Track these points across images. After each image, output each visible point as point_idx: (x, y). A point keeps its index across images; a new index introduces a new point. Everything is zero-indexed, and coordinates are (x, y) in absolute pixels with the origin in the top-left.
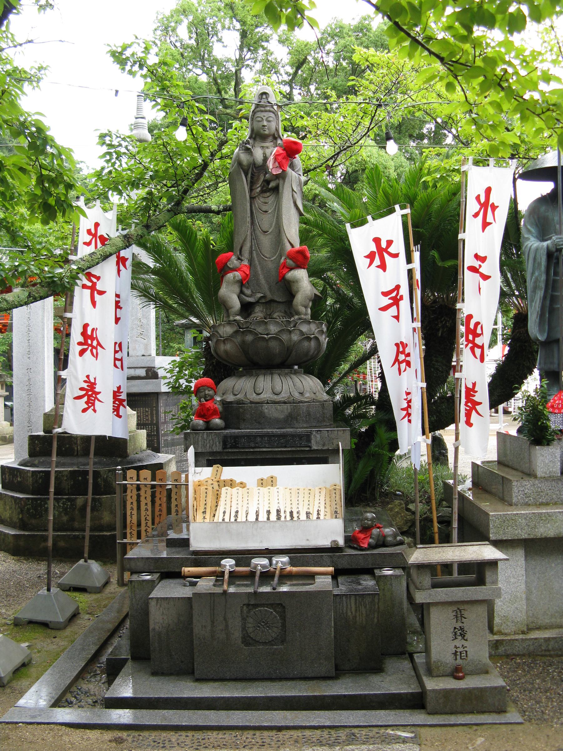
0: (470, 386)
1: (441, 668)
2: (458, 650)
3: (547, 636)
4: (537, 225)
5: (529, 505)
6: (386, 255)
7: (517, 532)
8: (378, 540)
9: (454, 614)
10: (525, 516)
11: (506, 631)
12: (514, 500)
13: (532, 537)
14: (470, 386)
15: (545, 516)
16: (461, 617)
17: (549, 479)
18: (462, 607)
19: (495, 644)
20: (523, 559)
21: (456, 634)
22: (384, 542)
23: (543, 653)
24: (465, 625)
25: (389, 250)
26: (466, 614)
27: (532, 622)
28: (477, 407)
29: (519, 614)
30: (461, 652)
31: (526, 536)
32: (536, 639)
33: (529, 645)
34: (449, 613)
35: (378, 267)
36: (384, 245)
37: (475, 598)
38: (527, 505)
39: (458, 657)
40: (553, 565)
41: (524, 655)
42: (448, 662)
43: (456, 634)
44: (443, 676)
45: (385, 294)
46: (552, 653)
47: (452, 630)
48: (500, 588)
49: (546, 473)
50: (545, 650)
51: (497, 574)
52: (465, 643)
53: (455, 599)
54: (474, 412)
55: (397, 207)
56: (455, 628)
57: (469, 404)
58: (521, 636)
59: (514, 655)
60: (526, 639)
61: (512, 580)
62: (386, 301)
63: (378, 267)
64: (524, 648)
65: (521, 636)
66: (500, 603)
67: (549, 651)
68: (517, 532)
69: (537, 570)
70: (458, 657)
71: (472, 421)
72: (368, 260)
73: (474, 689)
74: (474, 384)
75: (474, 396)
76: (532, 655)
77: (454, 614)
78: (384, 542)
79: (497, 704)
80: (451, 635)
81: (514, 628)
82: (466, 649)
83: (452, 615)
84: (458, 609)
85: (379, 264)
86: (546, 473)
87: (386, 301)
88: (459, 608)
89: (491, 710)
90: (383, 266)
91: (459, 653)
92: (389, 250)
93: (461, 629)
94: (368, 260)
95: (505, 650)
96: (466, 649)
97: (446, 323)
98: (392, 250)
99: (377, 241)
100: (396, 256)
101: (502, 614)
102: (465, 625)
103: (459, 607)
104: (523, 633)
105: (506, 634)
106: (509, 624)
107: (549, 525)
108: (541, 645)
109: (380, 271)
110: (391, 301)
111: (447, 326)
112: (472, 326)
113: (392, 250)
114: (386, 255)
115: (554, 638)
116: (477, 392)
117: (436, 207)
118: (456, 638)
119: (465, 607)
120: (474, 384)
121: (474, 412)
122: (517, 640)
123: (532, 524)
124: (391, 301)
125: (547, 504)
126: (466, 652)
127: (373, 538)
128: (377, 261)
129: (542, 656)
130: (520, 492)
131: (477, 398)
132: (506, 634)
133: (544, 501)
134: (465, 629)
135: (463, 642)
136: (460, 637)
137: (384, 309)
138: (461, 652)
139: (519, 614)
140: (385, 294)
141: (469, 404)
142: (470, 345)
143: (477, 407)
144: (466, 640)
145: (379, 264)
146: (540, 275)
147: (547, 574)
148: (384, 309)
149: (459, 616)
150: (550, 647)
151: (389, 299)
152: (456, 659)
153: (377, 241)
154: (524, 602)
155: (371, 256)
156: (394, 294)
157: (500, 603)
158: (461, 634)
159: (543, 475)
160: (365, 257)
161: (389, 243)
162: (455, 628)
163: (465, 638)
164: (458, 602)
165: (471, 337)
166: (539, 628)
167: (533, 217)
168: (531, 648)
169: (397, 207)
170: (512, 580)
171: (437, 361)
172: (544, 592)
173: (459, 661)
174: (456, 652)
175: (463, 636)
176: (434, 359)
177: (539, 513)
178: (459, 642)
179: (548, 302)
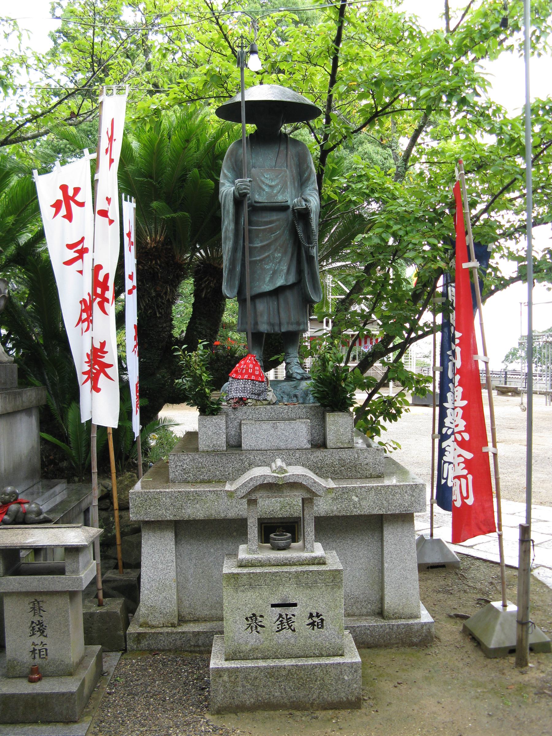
0: (98, 346)
1: (18, 668)
2: (37, 648)
3: (196, 630)
4: (234, 169)
5: (189, 482)
6: (72, 203)
7: (160, 512)
8: (16, 517)
9: (31, 605)
10: (170, 495)
11: (154, 623)
12: (171, 476)
13: (178, 518)
14: (98, 346)
15: (193, 496)
16: (40, 609)
17: (214, 452)
18: (40, 599)
19: (137, 637)
20: (173, 543)
21: (33, 628)
22: (24, 519)
23: (192, 648)
24: (44, 619)
25: (76, 198)
26: (45, 606)
27: (189, 614)
28: (107, 370)
29: (168, 604)
30: (39, 650)
31: (172, 518)
32: (183, 633)
33: (176, 640)
34: (26, 604)
35: (64, 217)
36: (71, 193)
37: (53, 588)
38: (186, 482)
39: (37, 656)
40: (212, 550)
41: (170, 650)
42: (25, 660)
43: (33, 628)
44: (19, 677)
45: (70, 247)
46: (202, 648)
47: (29, 625)
48: (81, 579)
49: (209, 446)
50: (194, 646)
51: (78, 562)
52: (45, 640)
53: (30, 589)
54: (102, 375)
55: (86, 151)
56: (33, 622)
57: (96, 367)
58: (169, 630)
59: (159, 650)
60: (172, 633)
61: (160, 566)
62: (71, 254)
63: (64, 217)
64: (170, 643)
65: (169, 630)
66: (146, 592)
67: (198, 646)
68: (160, 512)
69: (193, 556)
70: (37, 656)
71: (99, 386)
72: (54, 209)
73: (38, 694)
74: (103, 344)
75: (103, 357)
76: (177, 650)
77: (31, 605)
78: (24, 519)
79: (65, 712)
80: (28, 630)
81: (162, 620)
82: (45, 647)
83: (28, 607)
84: (36, 600)
85: (65, 213)
86: (209, 446)
87: (71, 254)
88: (37, 598)
89: (58, 719)
90: (69, 216)
91: (37, 651)
92: (76, 198)
93: (40, 623)
94: (54, 209)
95: (149, 644)
96: (45, 647)
97: (209, 283)
98: (78, 198)
99: (64, 188)
100: (81, 205)
101: (149, 603)
102: (44, 619)
103: (37, 598)
104: (173, 625)
105: (153, 627)
106: (157, 615)
107: (198, 505)
108: (190, 640)
109: (66, 221)
110: (77, 255)
111: (211, 287)
112: (101, 278)
113: (78, 198)
114: (72, 203)
115: (203, 633)
116: (107, 352)
117: (167, 155)
118: (33, 634)
119: (44, 598)
120: (103, 344)
121: (102, 375)
122: (161, 633)
123: (178, 504)
124: (77, 255)
125: (209, 482)
126: (46, 650)
127: (9, 515)
128: (63, 211)
129: (191, 652)
130: (178, 468)
131: (106, 360)
132: (153, 627)
133: (206, 478)
134: (45, 624)
135: (42, 639)
136: (39, 633)
137: (69, 263)
138: (39, 650)
139: (168, 604)
140: (70, 247)
141: (96, 367)
142: (98, 300)
143: (107, 370)
144: (46, 636)
145: (65, 213)
146: (229, 224)
147: (205, 560)
148: (69, 263)
149: (36, 608)
150: (200, 643)
151: (75, 252)
152: (34, 658)
153: (64, 188)
154: (174, 591)
155: (57, 205)
156: (79, 247)
157: (146, 592)
158: (40, 630)
159: (206, 449)
160: (52, 206)
161: (77, 190)
162: (33, 622)
163: (45, 634)
164: (36, 592)
165: (99, 291)
166: (196, 620)
167: (230, 160)
168: (179, 643)
169: (86, 151)
170: (160, 566)
171: (200, 324)
172: (203, 581)
173: (38, 660)
174: (35, 650)
175: (42, 631)
176: (198, 322)
177: (186, 492)
178: (37, 639)
179: (239, 255)
